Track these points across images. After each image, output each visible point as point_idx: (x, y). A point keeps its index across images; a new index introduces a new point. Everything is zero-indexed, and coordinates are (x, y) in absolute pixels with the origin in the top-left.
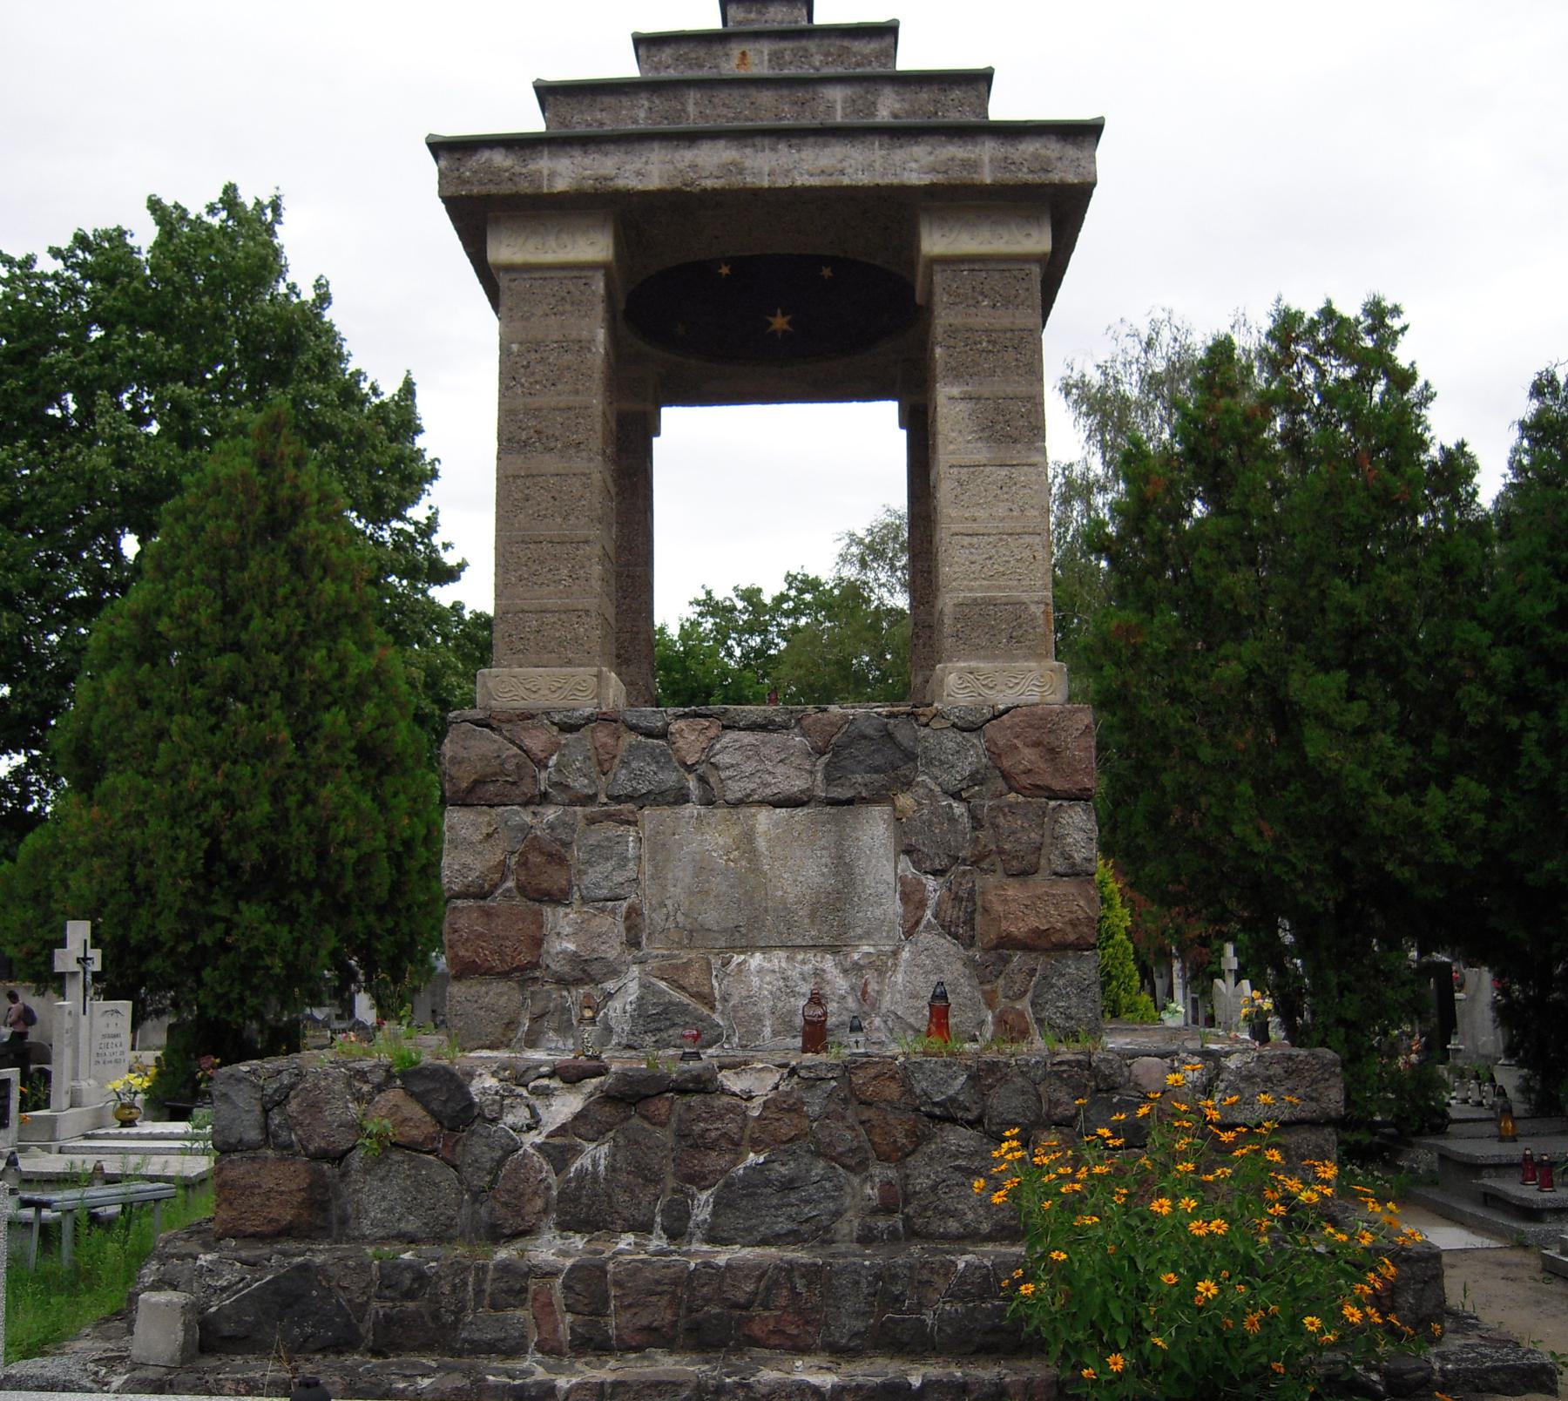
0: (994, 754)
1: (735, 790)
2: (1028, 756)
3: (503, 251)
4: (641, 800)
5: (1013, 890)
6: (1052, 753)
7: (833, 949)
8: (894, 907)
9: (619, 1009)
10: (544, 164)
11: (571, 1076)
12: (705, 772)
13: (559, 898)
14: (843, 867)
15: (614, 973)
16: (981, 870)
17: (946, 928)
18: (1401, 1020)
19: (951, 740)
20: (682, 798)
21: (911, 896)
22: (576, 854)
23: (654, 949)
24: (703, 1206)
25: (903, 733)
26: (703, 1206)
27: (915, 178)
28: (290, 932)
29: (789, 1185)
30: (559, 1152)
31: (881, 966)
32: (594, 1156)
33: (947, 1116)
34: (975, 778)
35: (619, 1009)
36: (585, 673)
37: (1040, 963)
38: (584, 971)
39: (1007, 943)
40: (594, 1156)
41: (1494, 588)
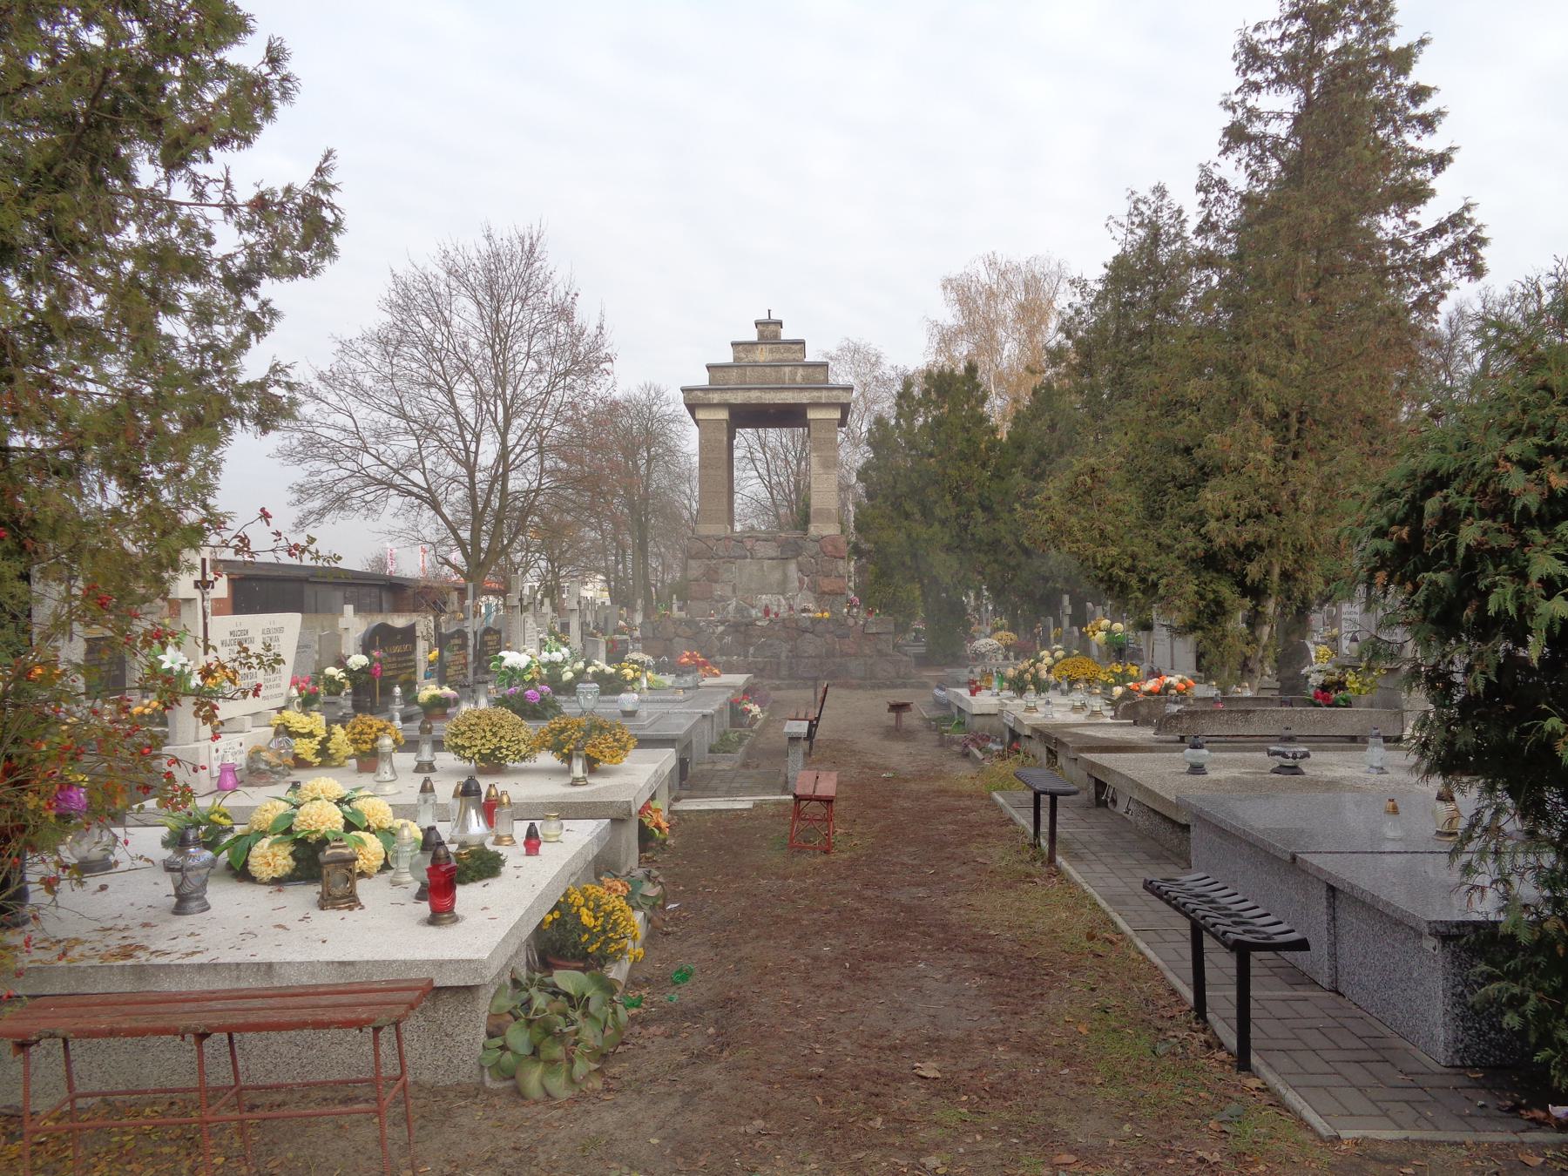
0: (821, 548)
1: (759, 555)
2: (830, 548)
3: (701, 415)
4: (736, 558)
5: (826, 581)
6: (836, 547)
7: (783, 594)
8: (797, 584)
9: (731, 608)
10: (711, 395)
11: (722, 623)
12: (751, 551)
13: (716, 582)
14: (785, 576)
15: (729, 599)
16: (1376, 569)
17: (809, 589)
18: (190, 445)
19: (811, 544)
20: (746, 557)
21: (801, 581)
22: (720, 571)
23: (739, 594)
24: (751, 650)
25: (800, 542)
26: (751, 650)
27: (805, 401)
28: (69, 662)
29: (771, 645)
30: (721, 637)
31: (793, 598)
32: (728, 639)
33: (805, 631)
34: (817, 553)
35: (731, 608)
36: (721, 526)
37: (831, 598)
38: (722, 599)
39: (824, 593)
40: (728, 639)
41: (282, 748)
